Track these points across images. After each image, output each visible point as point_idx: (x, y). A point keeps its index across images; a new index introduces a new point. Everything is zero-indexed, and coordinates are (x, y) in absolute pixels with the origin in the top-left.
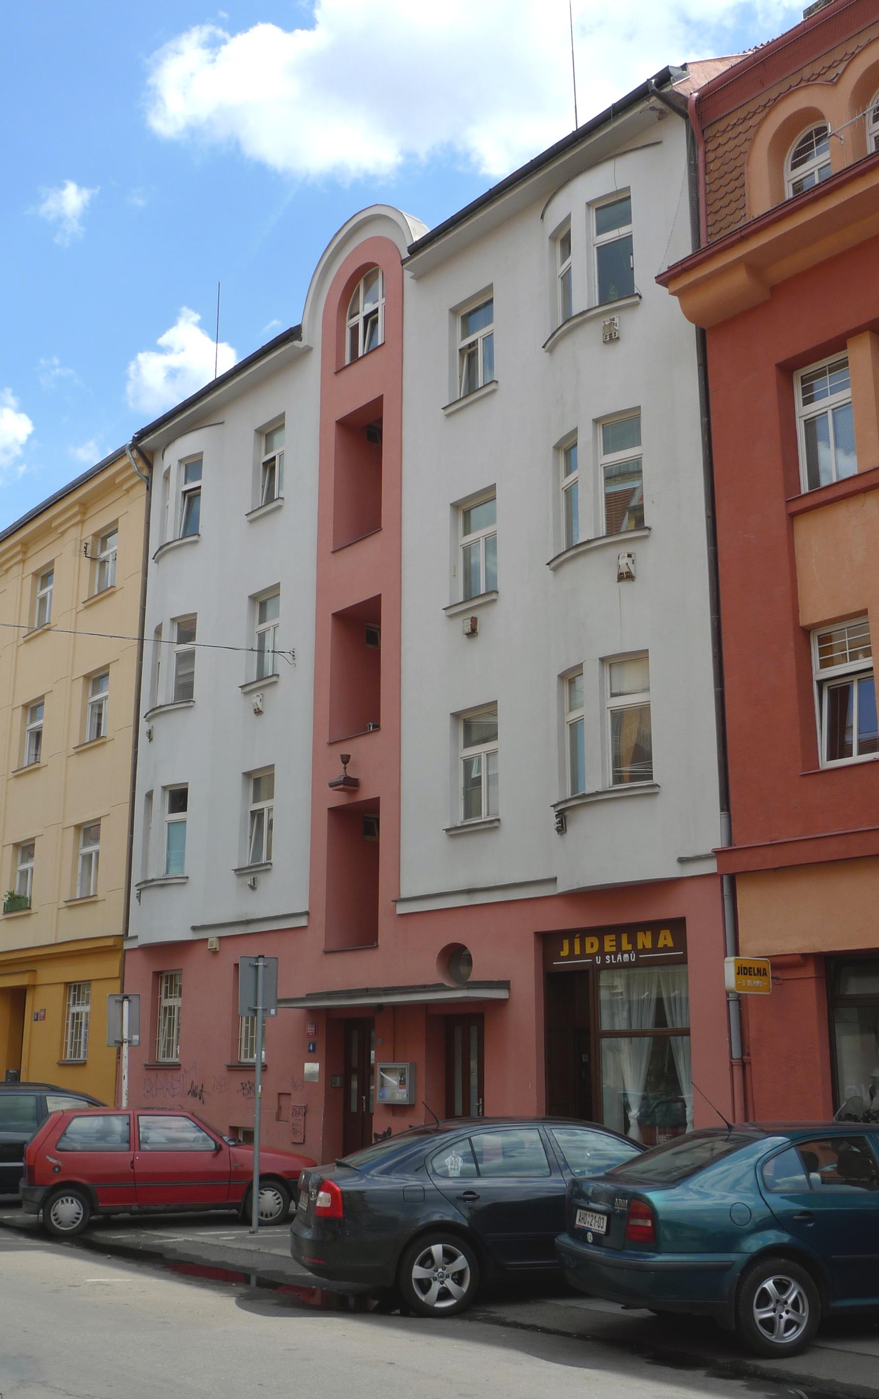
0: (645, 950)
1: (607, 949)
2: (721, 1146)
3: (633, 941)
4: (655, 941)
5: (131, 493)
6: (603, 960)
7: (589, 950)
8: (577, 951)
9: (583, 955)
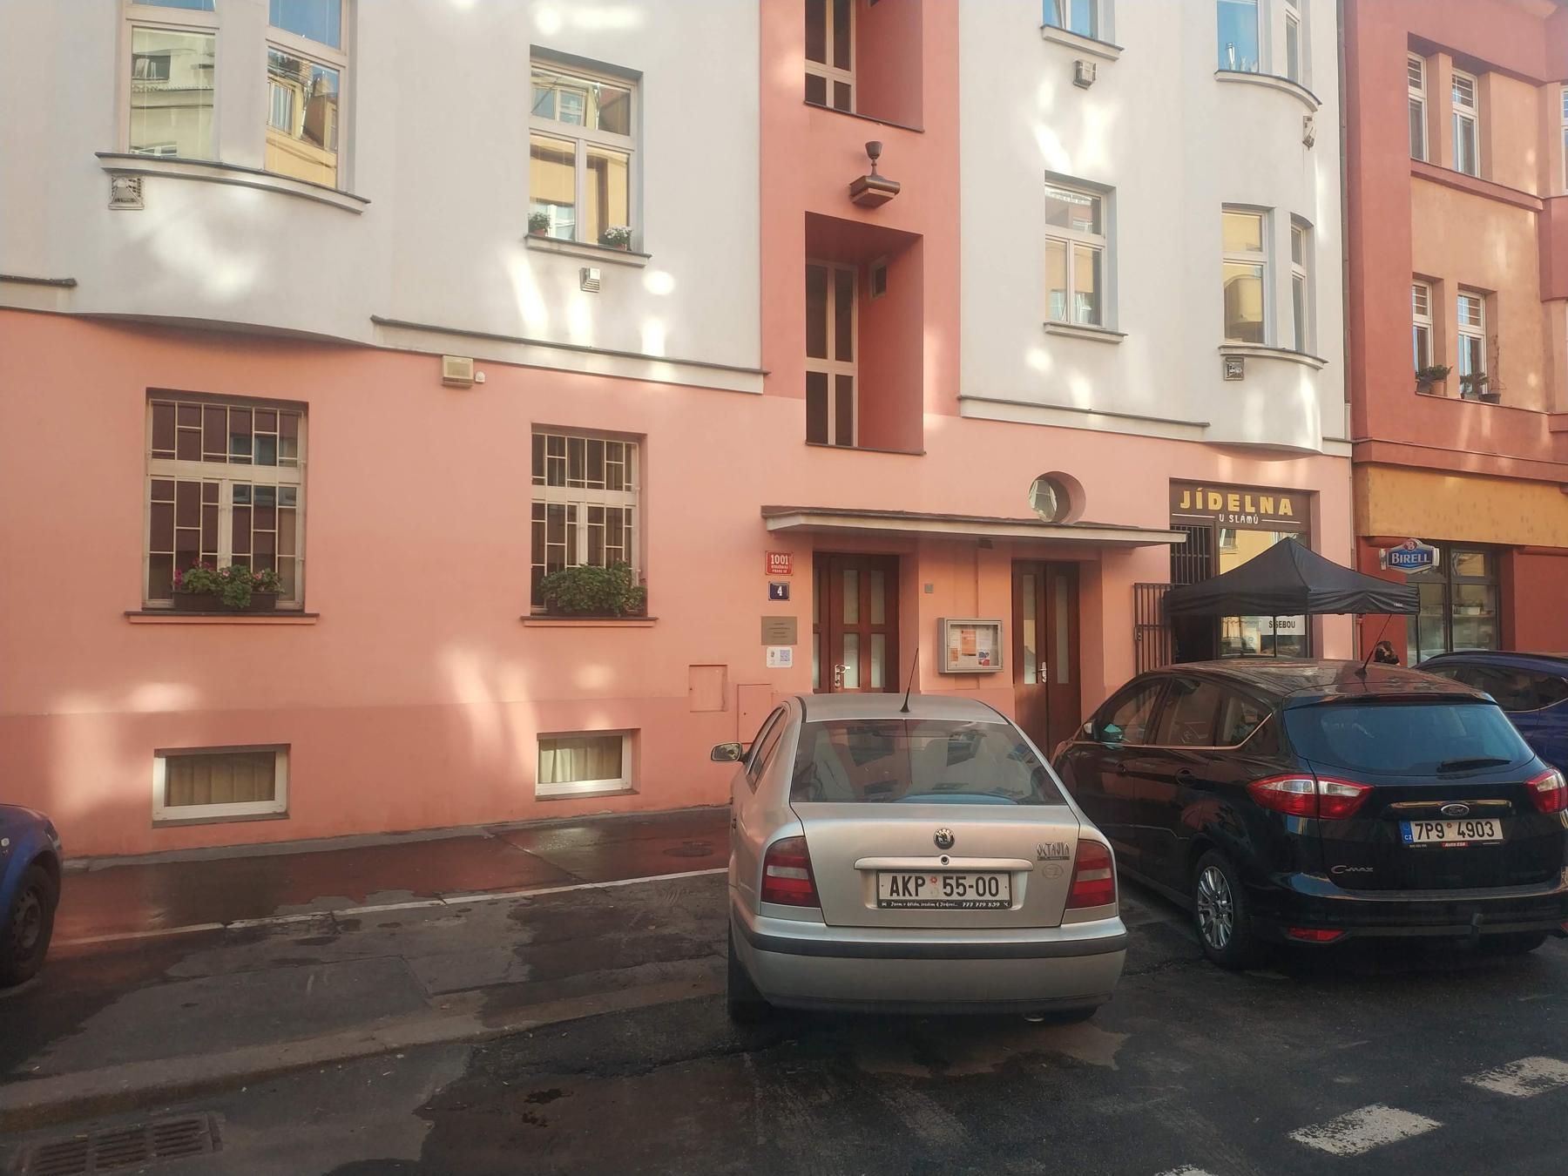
0: (1267, 515)
1: (1231, 508)
2: (1334, 724)
3: (1255, 504)
4: (1276, 507)
5: (1050, 45)
6: (1227, 519)
7: (1211, 506)
8: (1199, 506)
9: (1205, 510)
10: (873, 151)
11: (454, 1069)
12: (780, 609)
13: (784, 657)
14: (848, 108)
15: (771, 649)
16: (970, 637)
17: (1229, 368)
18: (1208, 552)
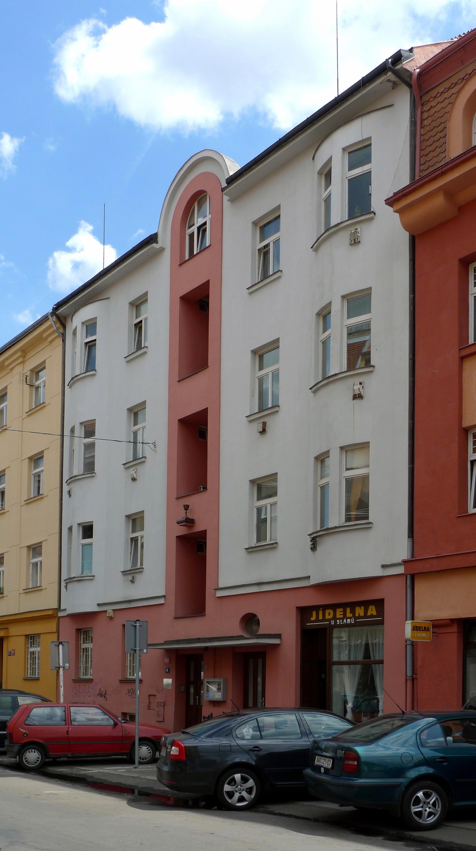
0: (360, 617)
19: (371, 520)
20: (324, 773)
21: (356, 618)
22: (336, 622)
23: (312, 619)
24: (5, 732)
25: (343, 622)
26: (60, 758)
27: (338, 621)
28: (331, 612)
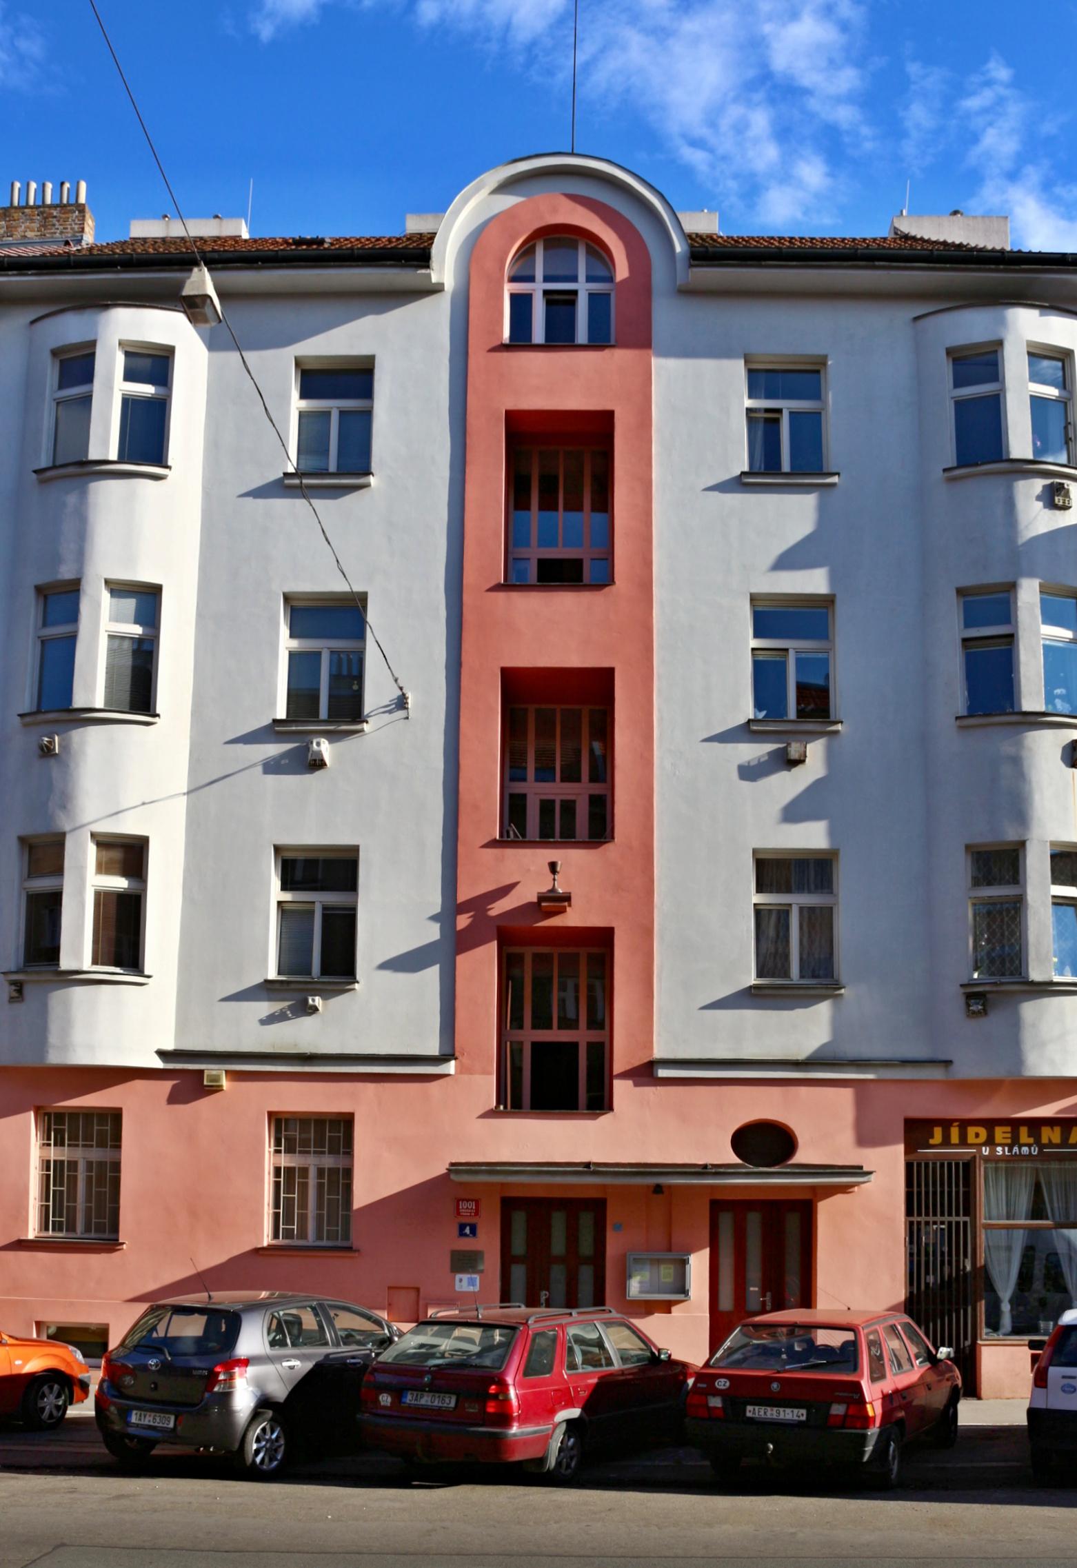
0: (1050, 1145)
10: (553, 867)
11: (594, 1381)
12: (467, 1244)
13: (472, 1282)
14: (317, 714)
15: (458, 1276)
16: (489, 1333)
17: (968, 1005)
18: (911, 1223)
19: (962, 990)
20: (548, 1289)
21: (1041, 1146)
22: (993, 1151)
23: (932, 1142)
24: (792, 713)
25: (1010, 1150)
26: (1067, 424)
27: (999, 1149)
28: (983, 1132)
